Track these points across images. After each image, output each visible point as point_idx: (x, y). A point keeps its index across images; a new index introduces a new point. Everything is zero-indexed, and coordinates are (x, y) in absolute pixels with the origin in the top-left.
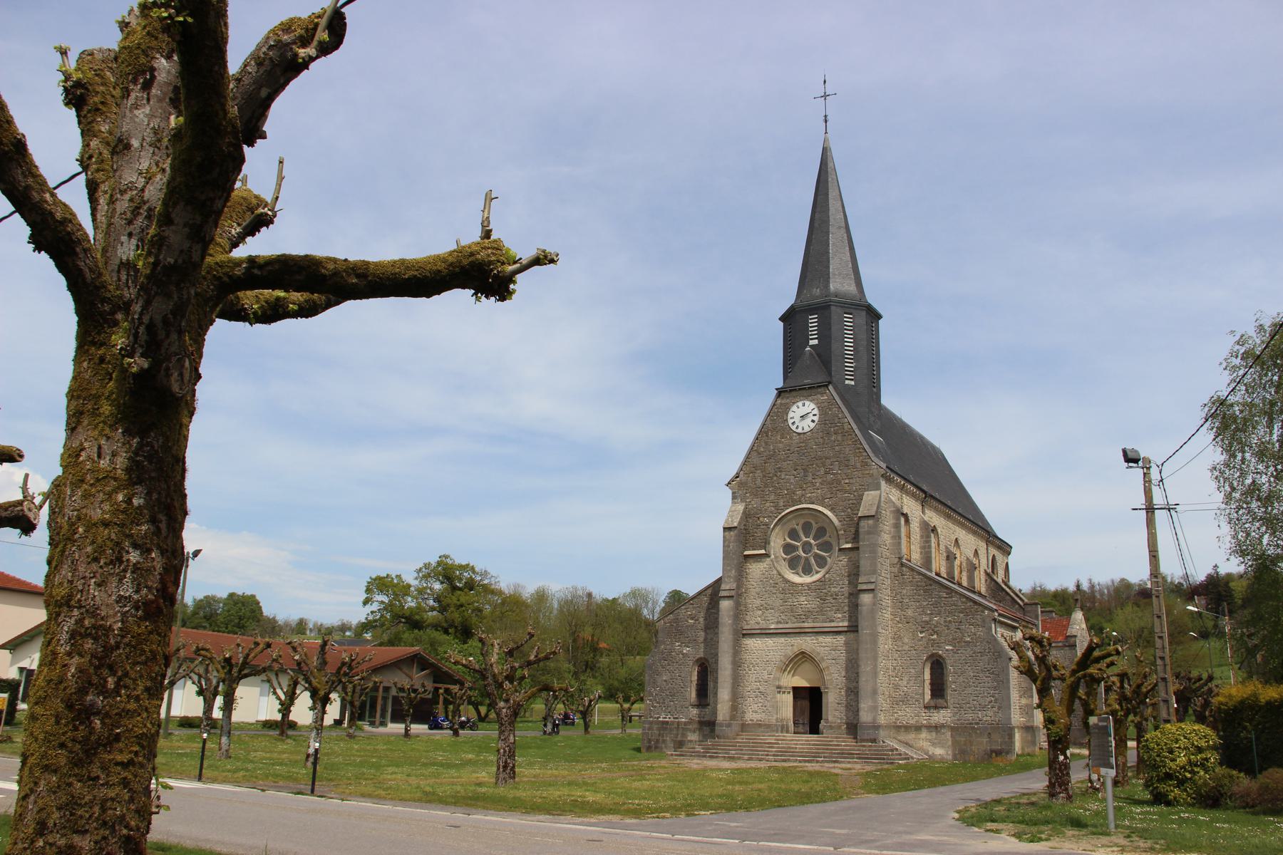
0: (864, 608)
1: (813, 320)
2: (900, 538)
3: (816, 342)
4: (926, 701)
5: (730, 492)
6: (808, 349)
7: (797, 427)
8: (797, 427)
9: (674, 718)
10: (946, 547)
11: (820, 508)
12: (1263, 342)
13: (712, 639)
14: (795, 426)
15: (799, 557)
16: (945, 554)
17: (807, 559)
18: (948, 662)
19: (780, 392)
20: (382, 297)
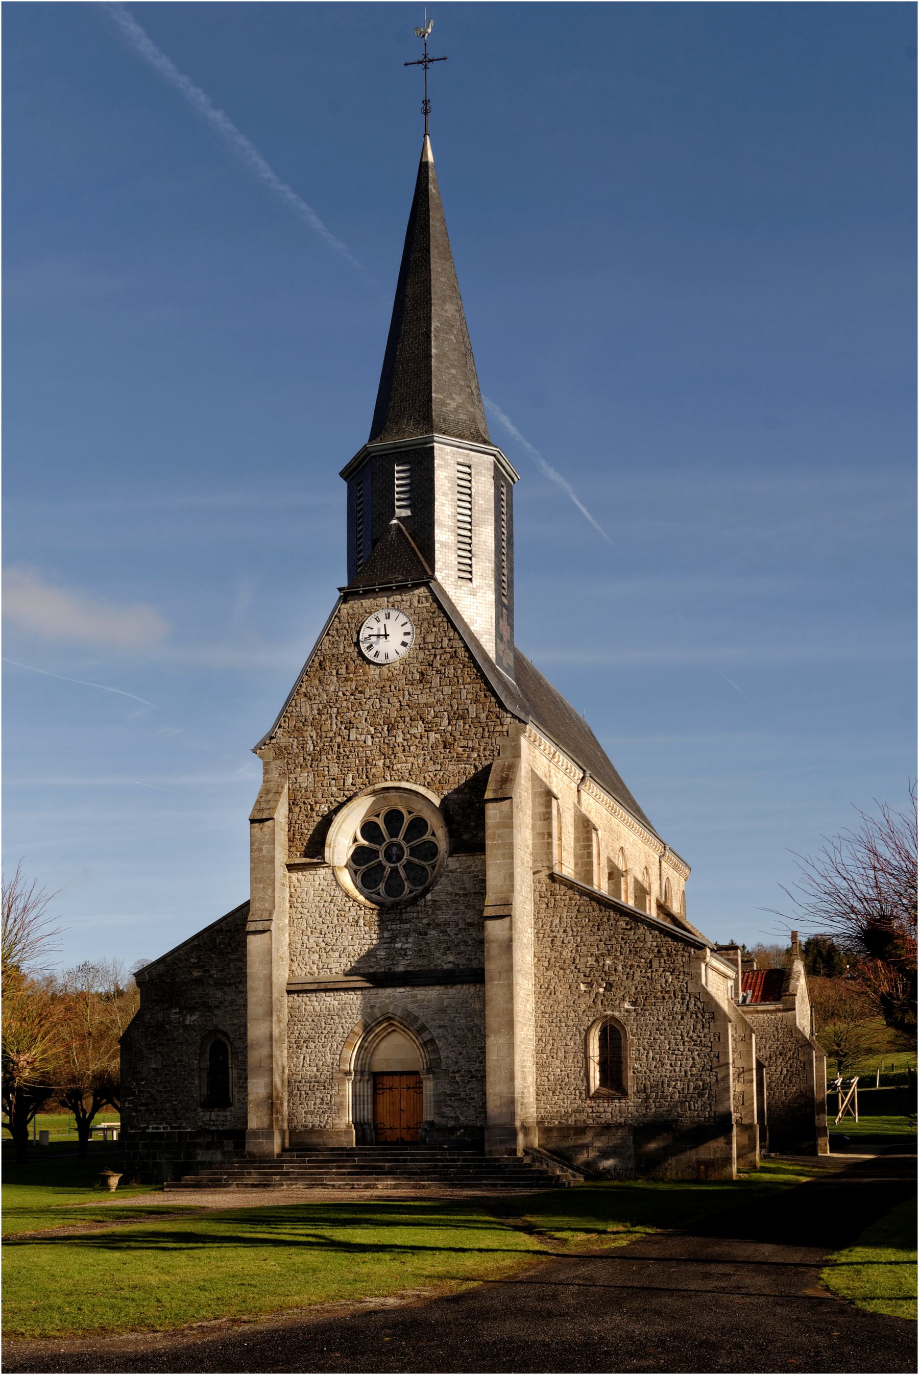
0: (494, 945)
1: (400, 474)
2: (550, 835)
3: (406, 513)
4: (593, 1090)
5: (261, 762)
6: (395, 522)
7: (377, 654)
8: (377, 654)
9: (172, 1128)
10: (609, 860)
11: (422, 790)
12: (582, 1081)
13: (232, 1002)
14: (373, 652)
15: (414, 851)
16: (606, 871)
17: (395, 871)
18: (628, 1029)
19: (346, 596)
20: (348, 511)
